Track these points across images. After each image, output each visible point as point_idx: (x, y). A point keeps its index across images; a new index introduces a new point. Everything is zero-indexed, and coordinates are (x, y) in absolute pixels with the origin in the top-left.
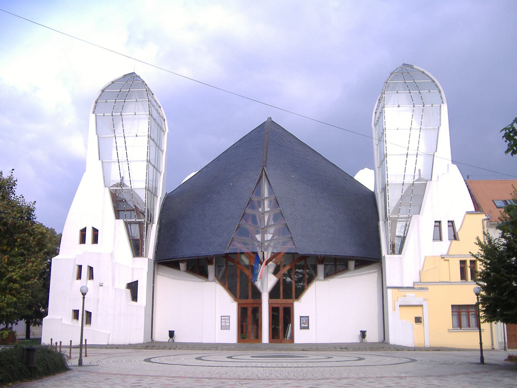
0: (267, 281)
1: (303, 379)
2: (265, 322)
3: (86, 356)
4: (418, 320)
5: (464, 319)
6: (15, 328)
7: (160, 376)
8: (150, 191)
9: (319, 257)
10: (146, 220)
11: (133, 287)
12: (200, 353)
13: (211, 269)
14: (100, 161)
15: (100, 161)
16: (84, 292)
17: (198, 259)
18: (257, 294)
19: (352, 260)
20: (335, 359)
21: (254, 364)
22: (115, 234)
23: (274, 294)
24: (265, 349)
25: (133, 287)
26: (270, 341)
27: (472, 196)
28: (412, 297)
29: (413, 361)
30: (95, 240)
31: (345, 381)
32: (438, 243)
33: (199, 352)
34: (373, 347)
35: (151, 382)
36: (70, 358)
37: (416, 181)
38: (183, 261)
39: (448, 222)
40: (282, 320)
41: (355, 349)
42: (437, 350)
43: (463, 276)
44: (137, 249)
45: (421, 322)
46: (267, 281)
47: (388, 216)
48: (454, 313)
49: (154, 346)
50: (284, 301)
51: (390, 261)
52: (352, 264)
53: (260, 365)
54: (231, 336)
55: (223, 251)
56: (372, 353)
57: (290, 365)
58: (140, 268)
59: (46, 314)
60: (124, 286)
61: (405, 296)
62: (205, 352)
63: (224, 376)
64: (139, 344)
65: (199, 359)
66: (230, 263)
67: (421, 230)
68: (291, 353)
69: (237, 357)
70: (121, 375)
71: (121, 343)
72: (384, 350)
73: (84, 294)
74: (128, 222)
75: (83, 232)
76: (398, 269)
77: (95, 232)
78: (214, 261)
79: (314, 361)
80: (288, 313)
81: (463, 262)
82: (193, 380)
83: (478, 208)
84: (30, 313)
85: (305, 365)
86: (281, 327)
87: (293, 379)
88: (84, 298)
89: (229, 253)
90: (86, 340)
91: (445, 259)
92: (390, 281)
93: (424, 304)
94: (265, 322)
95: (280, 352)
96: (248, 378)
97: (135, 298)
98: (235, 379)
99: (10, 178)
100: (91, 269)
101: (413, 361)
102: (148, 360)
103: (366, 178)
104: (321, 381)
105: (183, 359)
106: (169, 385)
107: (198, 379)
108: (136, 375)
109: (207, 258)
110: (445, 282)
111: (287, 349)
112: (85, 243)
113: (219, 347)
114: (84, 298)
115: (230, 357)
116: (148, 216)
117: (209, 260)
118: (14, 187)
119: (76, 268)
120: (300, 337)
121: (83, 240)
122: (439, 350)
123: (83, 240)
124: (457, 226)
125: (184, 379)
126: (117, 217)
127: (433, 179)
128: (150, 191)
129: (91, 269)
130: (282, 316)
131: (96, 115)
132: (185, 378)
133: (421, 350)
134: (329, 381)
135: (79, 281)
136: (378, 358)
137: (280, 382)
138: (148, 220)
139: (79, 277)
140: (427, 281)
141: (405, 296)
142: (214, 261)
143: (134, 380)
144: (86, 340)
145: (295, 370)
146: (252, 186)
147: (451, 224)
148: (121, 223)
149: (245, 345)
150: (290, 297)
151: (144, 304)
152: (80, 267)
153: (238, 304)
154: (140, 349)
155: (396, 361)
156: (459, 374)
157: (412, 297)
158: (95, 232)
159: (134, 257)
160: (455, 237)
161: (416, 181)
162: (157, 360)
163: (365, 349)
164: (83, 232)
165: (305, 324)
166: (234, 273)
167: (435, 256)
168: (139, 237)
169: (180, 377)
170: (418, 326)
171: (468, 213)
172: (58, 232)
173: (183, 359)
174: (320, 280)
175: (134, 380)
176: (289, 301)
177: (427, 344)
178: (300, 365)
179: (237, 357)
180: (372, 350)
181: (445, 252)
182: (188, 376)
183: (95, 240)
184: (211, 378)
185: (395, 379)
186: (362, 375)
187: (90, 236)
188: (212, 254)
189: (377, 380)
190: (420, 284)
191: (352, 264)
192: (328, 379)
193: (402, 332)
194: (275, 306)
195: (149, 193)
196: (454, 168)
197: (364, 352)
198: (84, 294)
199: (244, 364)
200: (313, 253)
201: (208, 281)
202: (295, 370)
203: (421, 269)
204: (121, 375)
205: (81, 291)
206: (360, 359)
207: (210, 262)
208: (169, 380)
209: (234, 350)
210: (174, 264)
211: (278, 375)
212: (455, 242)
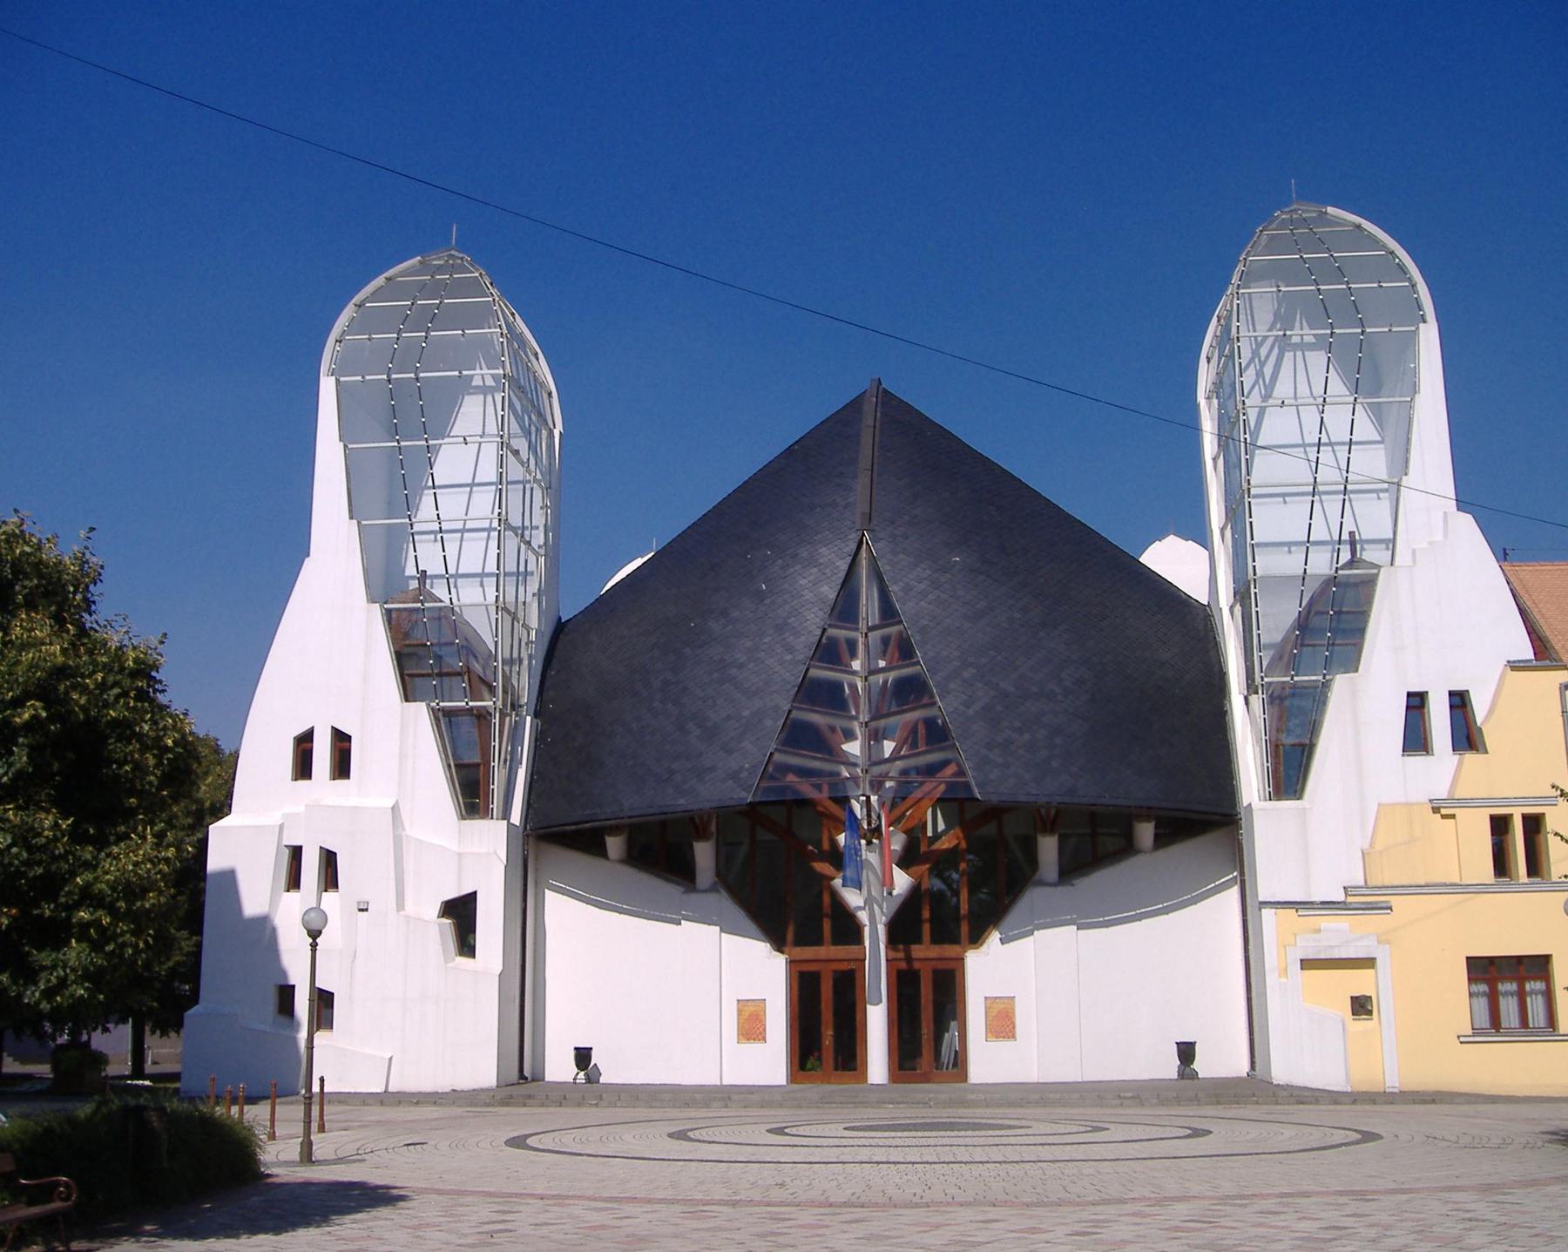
0: (873, 890)
1: (1039, 1204)
2: (881, 1016)
3: (322, 1129)
4: (1361, 1006)
5: (1508, 1007)
6: (98, 1041)
7: (567, 1197)
8: (508, 612)
9: (1043, 811)
10: (499, 704)
11: (461, 912)
12: (682, 1118)
16: (315, 926)
17: (663, 825)
18: (848, 929)
19: (1148, 819)
20: (1117, 1133)
21: (864, 1154)
22: (404, 747)
23: (902, 928)
24: (880, 1103)
25: (461, 912)
26: (793, 1077)
27: (1522, 611)
28: (1339, 935)
29: (1368, 1137)
30: (342, 767)
31: (1181, 1209)
32: (1417, 762)
33: (674, 1113)
34: (1226, 1092)
35: (543, 1218)
36: (272, 1136)
37: (1343, 568)
38: (614, 830)
40: (929, 1017)
41: (1163, 1102)
42: (1425, 1102)
43: (1501, 865)
44: (472, 793)
45: (1370, 1013)
46: (873, 890)
47: (1258, 680)
49: (529, 1097)
50: (934, 951)
51: (1268, 822)
52: (1145, 832)
53: (860, 1151)
54: (767, 1062)
55: (743, 794)
56: (1222, 1114)
57: (979, 1155)
58: (480, 854)
59: (194, 998)
60: (436, 908)
61: (1319, 931)
62: (693, 1113)
63: (777, 1195)
64: (482, 1090)
65: (681, 1135)
66: (763, 835)
68: (966, 1114)
69: (801, 1131)
70: (439, 1192)
71: (427, 1086)
72: (1257, 1103)
73: (314, 934)
74: (443, 710)
75: (304, 744)
76: (1292, 844)
77: (341, 741)
78: (713, 828)
79: (1051, 1139)
80: (949, 986)
81: (1500, 825)
82: (678, 1208)
83: (1544, 653)
84: (876, 770)
85: (1030, 1153)
86: (926, 1030)
87: (1005, 1204)
88: (314, 946)
89: (760, 803)
90: (322, 1080)
91: (1443, 811)
92: (1266, 888)
93: (1380, 954)
94: (881, 1016)
95: (925, 1112)
96: (854, 1199)
97: (466, 946)
98: (812, 1204)
99: (82, 562)
101: (1368, 1137)
102: (518, 1142)
103: (1173, 560)
104: (1100, 1208)
105: (628, 1137)
106: (603, 1227)
107: (695, 1207)
108: (490, 1194)
109: (692, 819)
110: (1445, 885)
111: (950, 1103)
112: (310, 777)
113: (735, 1097)
114: (314, 946)
115: (780, 1131)
116: (505, 692)
117: (696, 825)
118: (92, 587)
120: (988, 1061)
121: (303, 769)
122: (1433, 1101)
123: (303, 769)
124: (1480, 708)
125: (648, 1208)
126: (408, 696)
127: (1397, 562)
128: (508, 612)
130: (831, 1002)
131: (337, 381)
132: (649, 1201)
133: (1374, 1102)
134: (1128, 1208)
135: (293, 895)
136: (1255, 1131)
137: (967, 1214)
138: (504, 705)
139: (294, 882)
140: (1387, 883)
141: (1319, 931)
142: (713, 828)
143: (485, 1211)
144: (322, 1080)
145: (1003, 1174)
146: (830, 592)
147: (1459, 702)
148: (420, 712)
149: (812, 1090)
150: (954, 940)
151: (497, 966)
152: (296, 852)
154: (488, 1105)
155: (1315, 1137)
156: (1548, 1182)
157: (1339, 935)
158: (341, 741)
161: (1343, 568)
162: (547, 1141)
163: (1195, 1100)
164: (304, 744)
165: (1003, 1024)
166: (766, 868)
167: (1408, 805)
168: (476, 759)
169: (633, 1199)
170: (1362, 1025)
171: (1515, 666)
172: (227, 748)
173: (628, 1137)
174: (1042, 883)
175: (485, 1211)
176: (950, 950)
177: (1393, 1081)
178: (1011, 1154)
179: (801, 1131)
180: (1218, 1103)
181: (1442, 792)
182: (660, 1195)
183: (342, 767)
184: (735, 1204)
185: (1343, 1200)
186: (1228, 1188)
187: (326, 754)
188: (707, 805)
189: (1288, 1205)
190: (1365, 891)
191: (1145, 832)
192: (1122, 1201)
193: (1313, 1046)
195: (508, 619)
196: (1467, 521)
197: (1209, 1110)
198: (314, 934)
199: (831, 1154)
200: (1022, 798)
202: (1003, 1174)
203: (1366, 846)
204: (439, 1192)
205: (305, 924)
206: (1197, 1133)
207: (702, 834)
208: (601, 1209)
209: (781, 1106)
210: (588, 841)
211: (953, 1191)
212: (1470, 757)
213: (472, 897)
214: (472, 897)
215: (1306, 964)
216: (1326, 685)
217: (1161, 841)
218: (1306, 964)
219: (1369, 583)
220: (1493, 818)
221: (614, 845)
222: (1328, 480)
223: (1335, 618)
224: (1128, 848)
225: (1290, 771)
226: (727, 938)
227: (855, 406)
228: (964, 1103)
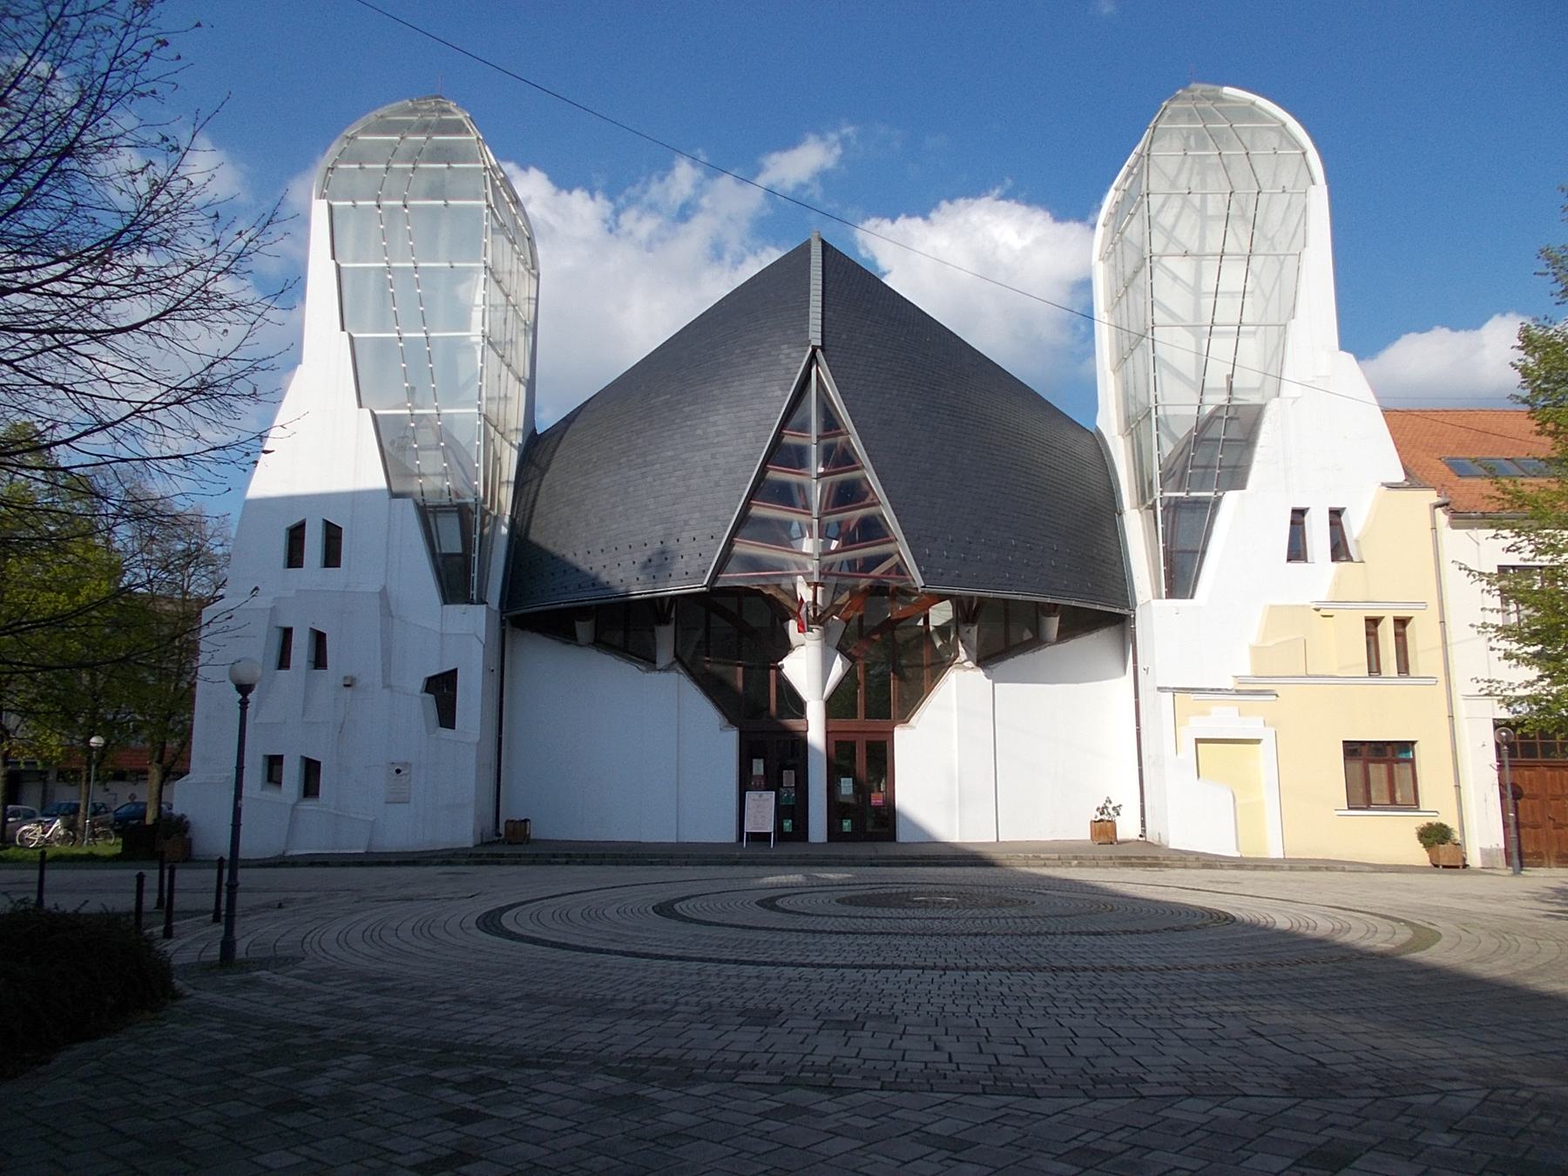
0: (808, 668)
11: (442, 687)
13: (665, 639)
14: (345, 334)
15: (345, 334)
23: (837, 705)
25: (442, 687)
30: (332, 557)
39: (1496, 727)
48: (1379, 791)
52: (1053, 625)
60: (419, 684)
67: (1243, 526)
81: (1403, 667)
88: (244, 704)
91: (1323, 612)
97: (447, 717)
100: (319, 639)
114: (244, 704)
119: (277, 639)
121: (294, 557)
123: (294, 557)
124: (1353, 527)
129: (319, 639)
152: (287, 632)
153: (741, 733)
157: (1224, 719)
159: (445, 602)
160: (1339, 550)
176: (877, 724)
183: (332, 557)
191: (1053, 625)
194: (844, 738)
201: (655, 669)
213: (455, 671)
214: (455, 671)
215: (1258, 741)
216: (1220, 498)
217: (1066, 634)
218: (1258, 741)
219: (1257, 413)
220: (1368, 620)
221: (584, 629)
222: (1223, 321)
223: (1221, 448)
224: (1037, 642)
225: (1180, 577)
226: (1139, 602)
227: (805, 249)
228: (890, 862)
